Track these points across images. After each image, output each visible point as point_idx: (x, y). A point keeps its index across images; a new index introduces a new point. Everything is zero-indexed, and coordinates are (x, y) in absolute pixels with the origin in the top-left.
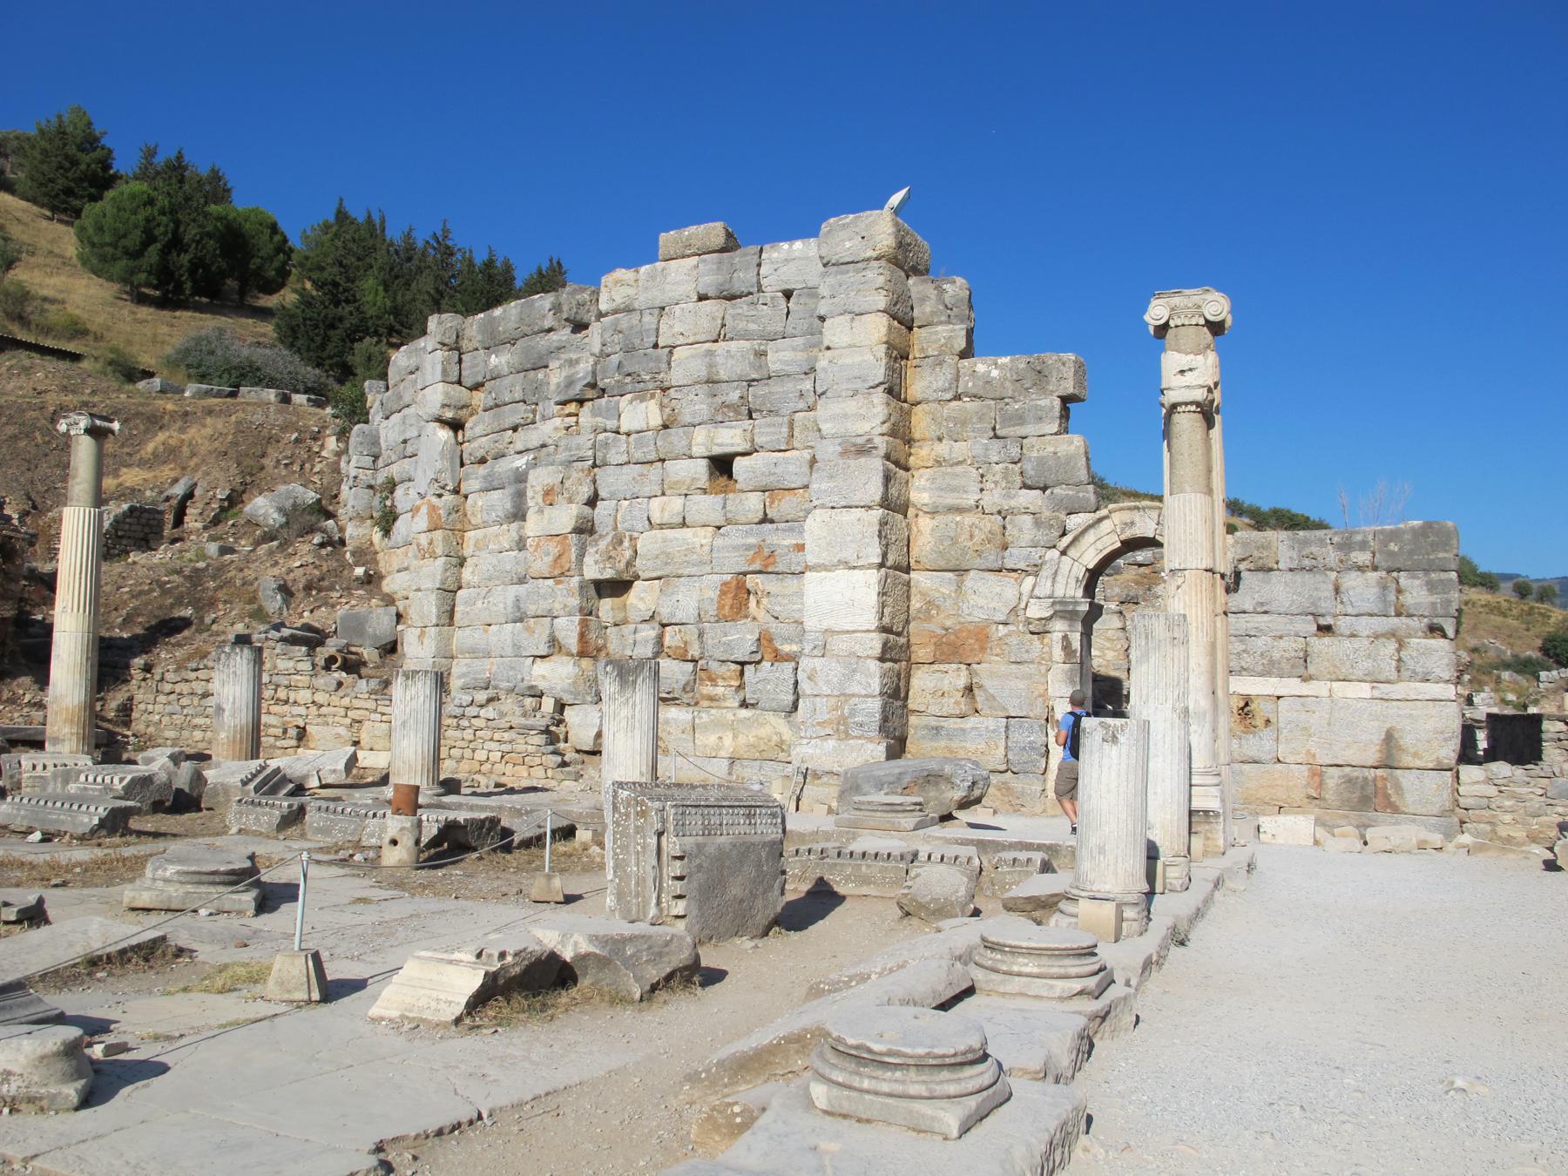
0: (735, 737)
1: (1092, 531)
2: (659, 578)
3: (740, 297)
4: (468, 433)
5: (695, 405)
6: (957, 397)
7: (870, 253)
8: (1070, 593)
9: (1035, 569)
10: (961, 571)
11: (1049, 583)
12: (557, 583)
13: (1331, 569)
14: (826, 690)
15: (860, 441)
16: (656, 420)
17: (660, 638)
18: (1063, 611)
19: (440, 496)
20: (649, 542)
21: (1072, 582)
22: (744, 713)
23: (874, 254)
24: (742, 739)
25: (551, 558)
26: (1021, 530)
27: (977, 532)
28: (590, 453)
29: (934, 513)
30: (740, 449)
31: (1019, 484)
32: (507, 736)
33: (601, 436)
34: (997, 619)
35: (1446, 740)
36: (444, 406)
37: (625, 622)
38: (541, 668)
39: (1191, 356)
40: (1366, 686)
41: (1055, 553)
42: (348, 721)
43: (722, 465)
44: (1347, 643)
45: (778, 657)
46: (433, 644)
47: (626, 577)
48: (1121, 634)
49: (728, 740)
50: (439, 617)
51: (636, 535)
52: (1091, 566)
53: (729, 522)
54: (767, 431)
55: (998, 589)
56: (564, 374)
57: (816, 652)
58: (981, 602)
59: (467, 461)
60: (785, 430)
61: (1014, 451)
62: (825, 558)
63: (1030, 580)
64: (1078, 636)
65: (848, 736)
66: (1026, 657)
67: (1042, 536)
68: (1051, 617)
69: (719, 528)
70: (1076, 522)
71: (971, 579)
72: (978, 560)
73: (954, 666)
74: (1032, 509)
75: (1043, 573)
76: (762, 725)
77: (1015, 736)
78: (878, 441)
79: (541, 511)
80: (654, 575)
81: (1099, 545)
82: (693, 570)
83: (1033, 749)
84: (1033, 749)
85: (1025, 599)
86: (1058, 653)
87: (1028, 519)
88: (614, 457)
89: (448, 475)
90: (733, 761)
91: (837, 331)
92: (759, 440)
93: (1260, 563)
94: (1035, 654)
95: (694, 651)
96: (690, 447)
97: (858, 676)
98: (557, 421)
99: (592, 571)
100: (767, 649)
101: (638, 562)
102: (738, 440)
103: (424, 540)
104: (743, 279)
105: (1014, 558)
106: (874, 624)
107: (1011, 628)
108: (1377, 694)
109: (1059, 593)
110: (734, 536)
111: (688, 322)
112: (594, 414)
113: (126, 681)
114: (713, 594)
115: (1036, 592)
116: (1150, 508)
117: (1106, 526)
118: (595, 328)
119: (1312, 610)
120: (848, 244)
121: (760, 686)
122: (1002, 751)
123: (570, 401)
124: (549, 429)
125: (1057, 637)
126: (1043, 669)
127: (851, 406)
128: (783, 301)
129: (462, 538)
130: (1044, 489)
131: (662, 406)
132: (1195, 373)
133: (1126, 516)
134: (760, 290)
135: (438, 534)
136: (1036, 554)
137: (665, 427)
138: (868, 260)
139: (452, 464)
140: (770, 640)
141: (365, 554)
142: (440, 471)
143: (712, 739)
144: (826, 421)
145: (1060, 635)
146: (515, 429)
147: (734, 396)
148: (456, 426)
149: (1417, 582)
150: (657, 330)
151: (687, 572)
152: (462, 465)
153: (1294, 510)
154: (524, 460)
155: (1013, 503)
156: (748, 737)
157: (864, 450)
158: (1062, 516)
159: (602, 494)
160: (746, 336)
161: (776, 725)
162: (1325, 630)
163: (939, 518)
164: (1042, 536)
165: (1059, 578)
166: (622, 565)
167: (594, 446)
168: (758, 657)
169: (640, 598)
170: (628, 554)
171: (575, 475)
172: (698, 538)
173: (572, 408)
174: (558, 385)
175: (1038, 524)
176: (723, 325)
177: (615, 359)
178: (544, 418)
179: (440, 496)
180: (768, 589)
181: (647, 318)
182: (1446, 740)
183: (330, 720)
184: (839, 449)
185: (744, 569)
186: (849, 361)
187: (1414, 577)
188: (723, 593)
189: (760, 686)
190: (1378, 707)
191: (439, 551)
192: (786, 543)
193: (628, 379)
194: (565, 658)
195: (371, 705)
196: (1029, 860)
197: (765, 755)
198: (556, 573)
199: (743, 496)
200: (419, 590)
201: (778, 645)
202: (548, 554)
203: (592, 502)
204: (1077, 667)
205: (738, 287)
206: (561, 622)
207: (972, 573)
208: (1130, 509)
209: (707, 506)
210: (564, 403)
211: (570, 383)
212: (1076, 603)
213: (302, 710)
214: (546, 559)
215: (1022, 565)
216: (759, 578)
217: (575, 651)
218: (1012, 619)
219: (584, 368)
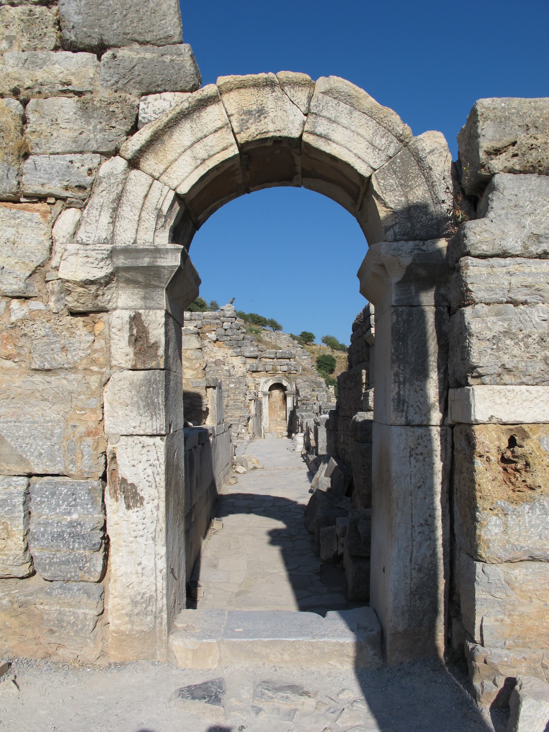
1: (186, 126)
9: (79, 196)
11: (105, 218)
18: (129, 269)
21: (150, 220)
26: (54, 122)
31: (52, 40)
41: (118, 164)
48: (198, 353)
52: (184, 189)
55: (10, 233)
63: (70, 216)
64: (159, 316)
66: (60, 358)
67: (96, 135)
68: (107, 281)
70: (158, 107)
74: (76, 86)
75: (96, 200)
77: (43, 512)
81: (201, 151)
83: (76, 536)
84: (76, 536)
86: (122, 351)
87: (69, 104)
93: (533, 157)
94: (77, 355)
107: (34, 305)
109: (124, 238)
116: (294, 84)
117: (213, 116)
122: (17, 543)
125: (119, 318)
126: (94, 381)
130: (99, 49)
133: (248, 99)
145: (126, 315)
153: (259, 315)
155: (40, 75)
164: (96, 135)
165: (125, 210)
175: (86, 110)
204: (160, 376)
208: (256, 85)
212: (157, 251)
218: (35, 288)
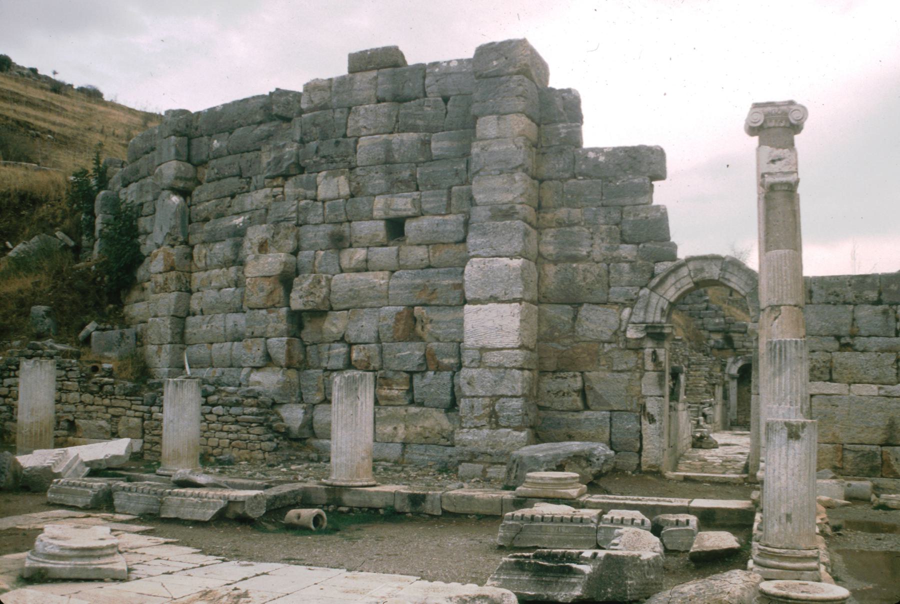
0: (406, 427)
2: (348, 309)
3: (410, 100)
4: (195, 199)
5: (378, 180)
6: (574, 176)
7: (511, 70)
8: (658, 319)
9: (632, 302)
10: (576, 304)
11: (642, 314)
12: (269, 312)
13: (850, 304)
14: (481, 392)
15: (504, 207)
16: (345, 190)
17: (349, 353)
19: (173, 246)
22: (413, 410)
24: (412, 429)
25: (265, 294)
27: (589, 275)
28: (294, 215)
29: (556, 262)
30: (410, 213)
32: (234, 427)
33: (303, 203)
34: (603, 339)
38: (256, 377)
39: (781, 150)
40: (875, 387)
41: (646, 291)
42: (109, 416)
43: (396, 228)
44: (862, 356)
45: (439, 368)
46: (168, 357)
47: (322, 308)
49: (401, 431)
50: (173, 337)
51: (330, 276)
52: (672, 300)
53: (401, 267)
54: (430, 200)
55: (604, 317)
56: (273, 155)
57: (473, 364)
58: (592, 326)
59: (194, 220)
60: (445, 199)
61: (615, 215)
62: (480, 294)
65: (498, 426)
69: (393, 272)
71: (584, 311)
72: (589, 296)
73: (571, 374)
75: (638, 305)
76: (427, 418)
80: (344, 306)
82: (375, 303)
85: (624, 323)
88: (312, 218)
89: (179, 229)
90: (405, 444)
91: (487, 126)
92: (426, 206)
96: (372, 210)
97: (505, 382)
98: (268, 191)
100: (429, 362)
102: (409, 206)
103: (160, 279)
105: (617, 293)
107: (614, 345)
108: (882, 392)
109: (650, 319)
110: (405, 277)
112: (296, 185)
115: (633, 319)
118: (297, 121)
119: (836, 332)
120: (495, 63)
121: (425, 389)
122: (607, 434)
123: (278, 176)
124: (258, 197)
126: (638, 375)
128: (442, 104)
129: (190, 277)
131: (350, 181)
132: (783, 162)
134: (425, 96)
135: (173, 274)
136: (632, 291)
137: (352, 196)
139: (183, 221)
140: (433, 356)
141: (753, 332)
142: (174, 227)
143: (389, 429)
144: (479, 193)
145: (651, 350)
146: (233, 196)
147: (406, 174)
148: (185, 193)
150: (346, 124)
151: (369, 304)
152: (190, 222)
154: (241, 219)
156: (416, 428)
157: (508, 214)
158: (651, 264)
159: (304, 245)
160: (414, 129)
161: (437, 420)
162: (844, 347)
163: (560, 265)
168: (424, 368)
169: (334, 325)
170: (325, 290)
171: (283, 231)
172: (378, 279)
173: (280, 181)
174: (269, 164)
175: (633, 269)
176: (397, 121)
177: (313, 145)
178: (256, 189)
179: (173, 246)
180: (431, 317)
181: (338, 115)
183: (94, 415)
184: (489, 213)
185: (412, 303)
186: (496, 148)
188: (397, 320)
189: (425, 389)
190: (883, 402)
191: (173, 287)
192: (446, 282)
193: (323, 161)
195: (126, 404)
196: (688, 522)
197: (429, 441)
198: (269, 304)
199: (412, 248)
200: (156, 316)
201: (438, 358)
202: (262, 290)
203: (295, 253)
206: (273, 341)
207: (585, 306)
209: (385, 254)
210: (273, 178)
211: (278, 161)
213: (72, 408)
214: (261, 294)
215: (621, 300)
216: (424, 311)
217: (283, 364)
219: (291, 149)
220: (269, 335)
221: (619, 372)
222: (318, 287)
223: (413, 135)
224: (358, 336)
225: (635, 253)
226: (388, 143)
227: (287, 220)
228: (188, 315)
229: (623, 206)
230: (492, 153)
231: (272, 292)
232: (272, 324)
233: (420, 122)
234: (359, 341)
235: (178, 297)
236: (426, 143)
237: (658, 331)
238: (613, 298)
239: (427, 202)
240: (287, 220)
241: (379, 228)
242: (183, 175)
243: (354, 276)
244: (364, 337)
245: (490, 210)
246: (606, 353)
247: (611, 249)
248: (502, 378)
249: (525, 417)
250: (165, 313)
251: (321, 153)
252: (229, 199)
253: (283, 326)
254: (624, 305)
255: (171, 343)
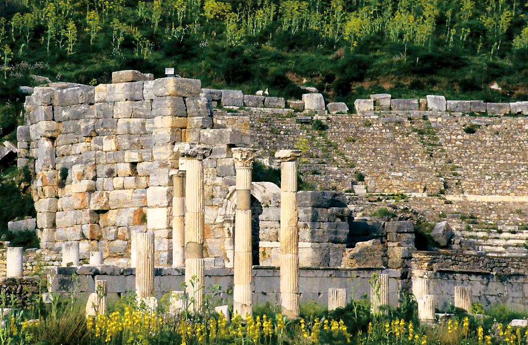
2: (116, 209)
7: (167, 93)
17: (117, 232)
20: (113, 195)
23: (168, 94)
25: (80, 201)
28: (93, 159)
33: (98, 152)
35: (309, 260)
36: (46, 131)
37: (107, 226)
41: (226, 200)
47: (105, 209)
51: (109, 192)
67: (222, 194)
68: (223, 222)
78: (169, 162)
79: (76, 182)
86: (227, 235)
95: (127, 237)
99: (94, 206)
101: (109, 203)
102: (137, 157)
104: (138, 94)
106: (165, 226)
111: (121, 110)
113: (518, 95)
114: (132, 215)
125: (226, 228)
127: (162, 149)
131: (116, 142)
138: (166, 96)
139: (51, 155)
142: (46, 160)
148: (53, 139)
149: (302, 211)
152: (56, 157)
159: (99, 175)
160: (140, 117)
166: (103, 205)
167: (95, 156)
169: (111, 216)
170: (105, 200)
172: (128, 193)
175: (221, 190)
176: (133, 112)
182: (309, 260)
185: (142, 205)
187: (301, 209)
188: (135, 214)
194: (86, 241)
198: (82, 207)
202: (79, 200)
203: (95, 179)
205: (136, 97)
220: (83, 223)
221: (218, 238)
222: (102, 198)
223: (139, 120)
224: (120, 223)
225: (222, 182)
226: (128, 123)
227: (90, 161)
228: (57, 211)
229: (217, 159)
230: (160, 135)
231: (83, 201)
232: (84, 217)
233: (141, 113)
234: (121, 225)
235: (50, 201)
236: (143, 124)
237: (229, 219)
238: (214, 204)
239: (144, 155)
240: (90, 161)
241: (127, 167)
242: (50, 129)
243: (119, 191)
244: (123, 223)
245: (159, 163)
246: (213, 230)
247: (213, 180)
248: (161, 243)
249: (333, 276)
250: (44, 210)
251: (104, 126)
252: (71, 145)
253: (88, 218)
254: (219, 207)
255: (47, 228)
